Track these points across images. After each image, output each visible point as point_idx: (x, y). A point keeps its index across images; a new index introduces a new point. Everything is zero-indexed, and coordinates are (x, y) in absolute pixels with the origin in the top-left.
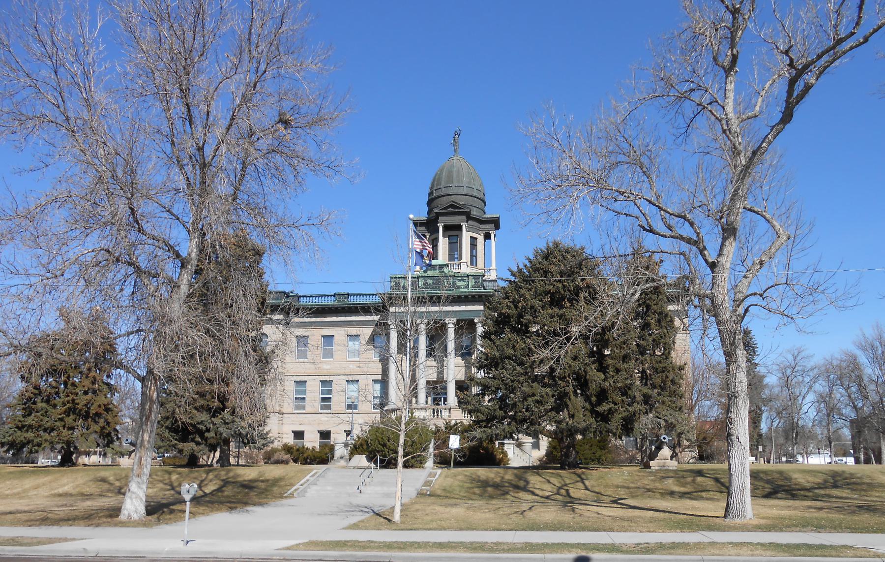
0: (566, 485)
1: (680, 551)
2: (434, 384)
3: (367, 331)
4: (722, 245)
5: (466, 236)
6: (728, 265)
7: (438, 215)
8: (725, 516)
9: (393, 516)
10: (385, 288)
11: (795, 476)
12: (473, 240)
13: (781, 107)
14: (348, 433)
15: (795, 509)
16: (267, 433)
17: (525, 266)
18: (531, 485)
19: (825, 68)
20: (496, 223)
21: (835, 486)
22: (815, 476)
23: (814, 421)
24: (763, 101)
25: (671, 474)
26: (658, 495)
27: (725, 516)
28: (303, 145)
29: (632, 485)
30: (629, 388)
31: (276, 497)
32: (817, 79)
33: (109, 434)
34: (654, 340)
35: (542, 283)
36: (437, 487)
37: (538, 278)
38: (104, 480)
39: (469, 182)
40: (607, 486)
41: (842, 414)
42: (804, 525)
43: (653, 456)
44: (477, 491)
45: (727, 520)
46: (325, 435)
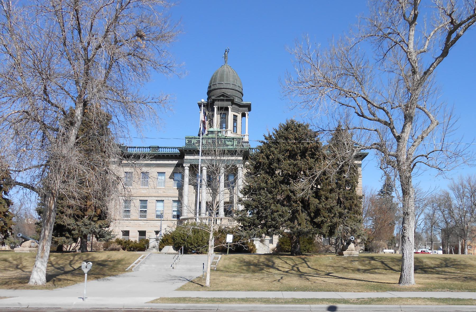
0: (296, 265)
1: (385, 303)
2: (216, 202)
3: (169, 171)
4: (404, 126)
5: (231, 114)
6: (407, 138)
7: (214, 101)
8: (399, 283)
9: (205, 283)
10: (182, 144)
11: (424, 260)
12: (235, 117)
13: (442, 47)
14: (157, 232)
15: (432, 279)
16: (111, 232)
17: (274, 134)
18: (276, 265)
19: (469, 26)
20: (249, 107)
21: (447, 266)
22: (435, 261)
23: (423, 230)
24: (429, 43)
25: (357, 259)
26: (351, 271)
27: (399, 283)
28: (150, 53)
29: (335, 265)
30: (332, 209)
31: (120, 271)
32: (464, 32)
33: (6, 231)
34: (346, 181)
35: (284, 145)
36: (220, 265)
37: (281, 141)
38: (5, 260)
39: (234, 81)
40: (320, 265)
41: (438, 226)
42: (443, 288)
43: (345, 248)
44: (244, 268)
45: (401, 285)
46: (142, 233)
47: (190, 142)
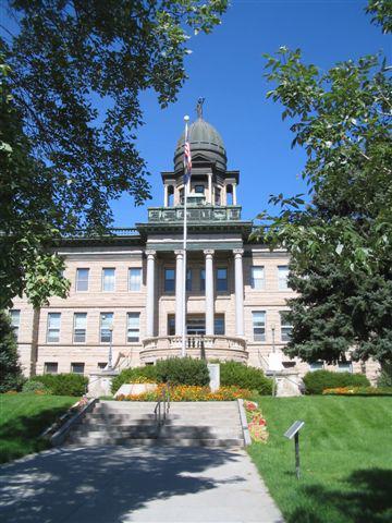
14: (102, 365)
47: (155, 215)
